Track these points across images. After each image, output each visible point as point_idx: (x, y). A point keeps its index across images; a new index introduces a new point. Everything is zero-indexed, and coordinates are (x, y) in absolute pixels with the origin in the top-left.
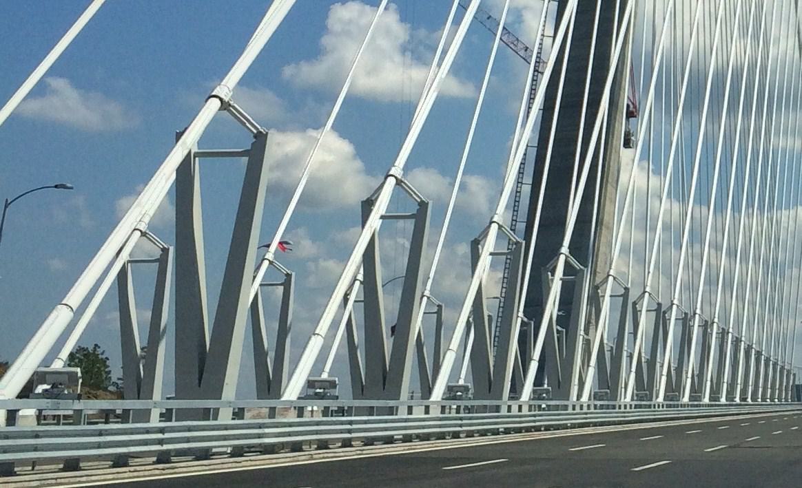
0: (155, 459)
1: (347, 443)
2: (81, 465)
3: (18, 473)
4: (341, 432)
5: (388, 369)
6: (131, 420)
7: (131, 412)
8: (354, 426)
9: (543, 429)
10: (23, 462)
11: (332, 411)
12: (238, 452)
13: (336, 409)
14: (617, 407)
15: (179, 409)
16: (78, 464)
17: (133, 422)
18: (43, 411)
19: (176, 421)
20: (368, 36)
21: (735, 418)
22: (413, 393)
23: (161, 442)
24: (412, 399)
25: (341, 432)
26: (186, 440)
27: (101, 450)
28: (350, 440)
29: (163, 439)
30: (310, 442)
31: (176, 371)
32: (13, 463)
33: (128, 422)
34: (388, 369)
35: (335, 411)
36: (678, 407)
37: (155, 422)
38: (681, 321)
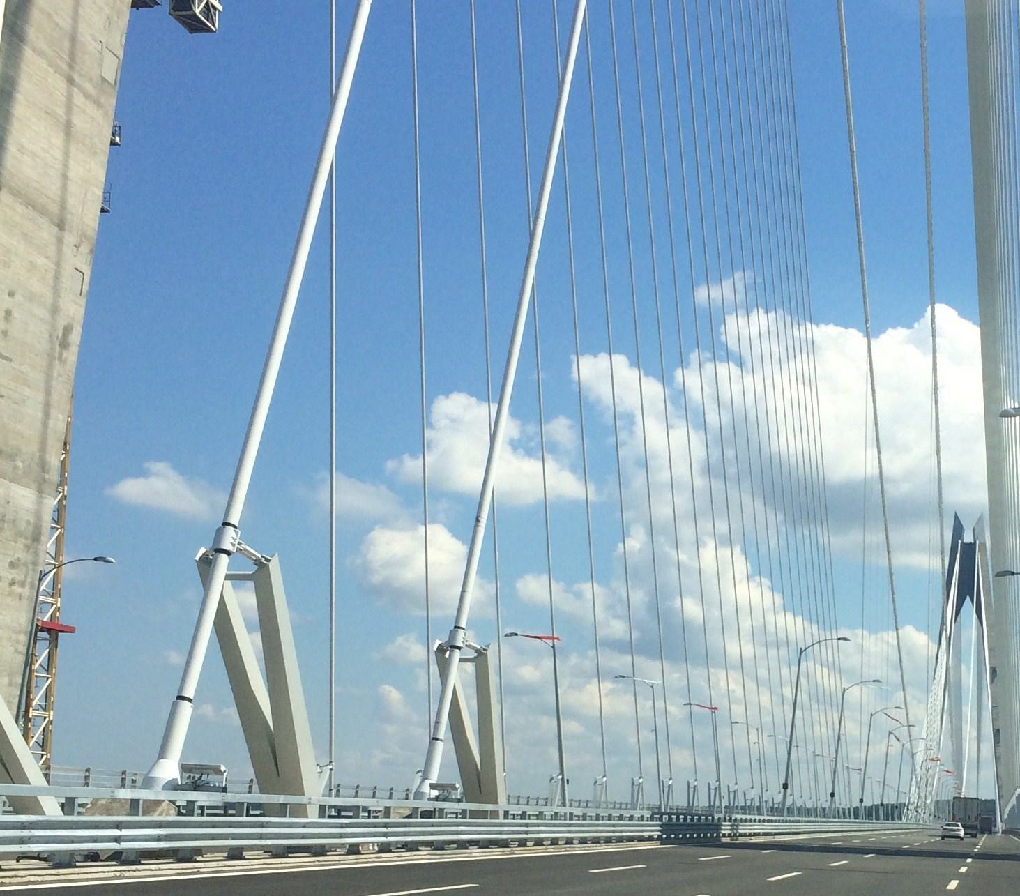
0: (226, 854)
1: (523, 843)
2: (244, 853)
3: (246, 857)
4: (520, 833)
5: (273, 729)
6: (141, 809)
7: (288, 806)
8: (530, 829)
9: (563, 842)
10: (251, 848)
11: (446, 812)
12: (385, 848)
13: (185, 804)
14: (501, 814)
15: (146, 800)
16: (242, 854)
17: (143, 815)
18: (76, 800)
19: (290, 817)
20: (966, 760)
21: (848, 834)
22: (88, 770)
23: (386, 835)
24: (87, 784)
25: (520, 833)
26: (301, 836)
27: (342, 839)
28: (526, 840)
29: (387, 833)
30: (513, 840)
31: (495, 778)
32: (242, 848)
33: (73, 815)
34: (273, 729)
35: (183, 806)
36: (191, 813)
37: (313, 817)
38: (973, 542)
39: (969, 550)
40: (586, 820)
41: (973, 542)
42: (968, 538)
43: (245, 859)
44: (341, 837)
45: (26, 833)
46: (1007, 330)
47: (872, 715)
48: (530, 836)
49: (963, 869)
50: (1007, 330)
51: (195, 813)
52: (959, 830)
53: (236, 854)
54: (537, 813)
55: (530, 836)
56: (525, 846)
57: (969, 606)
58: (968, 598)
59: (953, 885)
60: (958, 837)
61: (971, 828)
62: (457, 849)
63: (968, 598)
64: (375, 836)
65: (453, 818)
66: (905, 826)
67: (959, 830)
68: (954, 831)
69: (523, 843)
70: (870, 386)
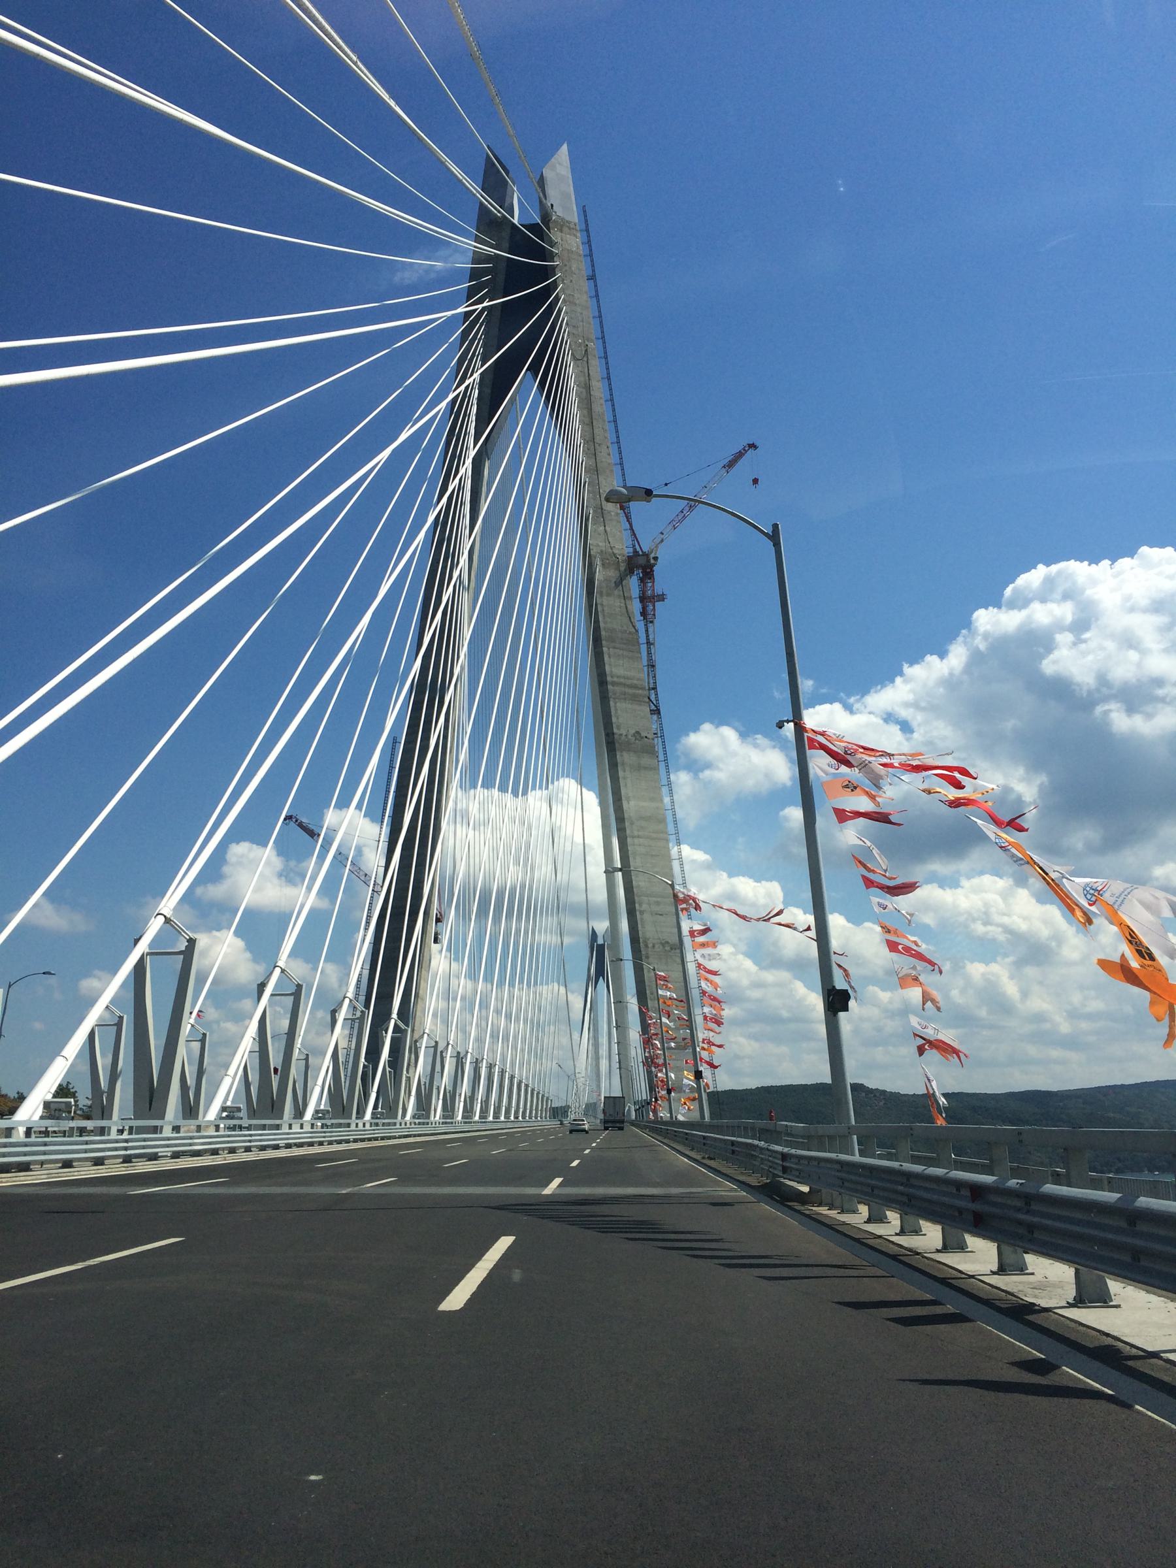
0: (121, 1160)
2: (74, 1164)
8: (253, 1138)
30: (223, 1149)
39: (601, 949)
40: (48, 1137)
41: (603, 943)
42: (600, 941)
43: (31, 1170)
44: (191, 1146)
45: (350, 1133)
46: (1059, 1218)
47: (10, 986)
48: (253, 1144)
49: (594, 1145)
50: (1059, 1218)
51: (75, 1134)
52: (584, 1124)
53: (67, 1164)
54: (247, 1126)
55: (253, 1144)
56: (323, 1145)
57: (601, 983)
58: (601, 978)
59: (587, 1151)
60: (584, 1130)
61: (611, 1122)
62: (60, 1168)
63: (601, 978)
64: (176, 1147)
65: (60, 1136)
66: (540, 1124)
67: (584, 1124)
68: (581, 1125)
69: (248, 1149)
70: (549, 809)
